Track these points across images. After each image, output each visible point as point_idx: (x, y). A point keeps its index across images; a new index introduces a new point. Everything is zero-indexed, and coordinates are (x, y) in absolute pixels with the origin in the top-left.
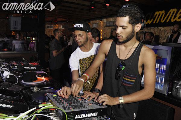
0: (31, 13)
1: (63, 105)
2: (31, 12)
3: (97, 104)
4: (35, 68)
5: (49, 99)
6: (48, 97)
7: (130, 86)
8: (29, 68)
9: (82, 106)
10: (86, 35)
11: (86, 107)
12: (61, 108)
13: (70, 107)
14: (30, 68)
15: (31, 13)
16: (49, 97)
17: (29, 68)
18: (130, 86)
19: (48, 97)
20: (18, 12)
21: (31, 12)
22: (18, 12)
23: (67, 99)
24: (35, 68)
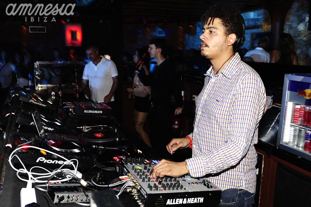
0: (52, 20)
1: (148, 183)
2: (54, 20)
3: (205, 185)
4: (101, 112)
5: (129, 172)
6: (127, 169)
7: (140, 138)
8: (91, 112)
9: (179, 186)
10: (227, 39)
11: (184, 187)
12: (145, 185)
13: (160, 186)
14: (93, 112)
15: (55, 20)
16: (128, 169)
17: (91, 112)
18: (140, 138)
19: (127, 169)
20: (32, 19)
21: (54, 20)
22: (32, 19)
23: (127, 164)
24: (101, 112)
